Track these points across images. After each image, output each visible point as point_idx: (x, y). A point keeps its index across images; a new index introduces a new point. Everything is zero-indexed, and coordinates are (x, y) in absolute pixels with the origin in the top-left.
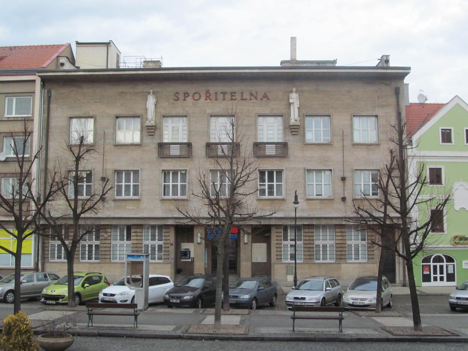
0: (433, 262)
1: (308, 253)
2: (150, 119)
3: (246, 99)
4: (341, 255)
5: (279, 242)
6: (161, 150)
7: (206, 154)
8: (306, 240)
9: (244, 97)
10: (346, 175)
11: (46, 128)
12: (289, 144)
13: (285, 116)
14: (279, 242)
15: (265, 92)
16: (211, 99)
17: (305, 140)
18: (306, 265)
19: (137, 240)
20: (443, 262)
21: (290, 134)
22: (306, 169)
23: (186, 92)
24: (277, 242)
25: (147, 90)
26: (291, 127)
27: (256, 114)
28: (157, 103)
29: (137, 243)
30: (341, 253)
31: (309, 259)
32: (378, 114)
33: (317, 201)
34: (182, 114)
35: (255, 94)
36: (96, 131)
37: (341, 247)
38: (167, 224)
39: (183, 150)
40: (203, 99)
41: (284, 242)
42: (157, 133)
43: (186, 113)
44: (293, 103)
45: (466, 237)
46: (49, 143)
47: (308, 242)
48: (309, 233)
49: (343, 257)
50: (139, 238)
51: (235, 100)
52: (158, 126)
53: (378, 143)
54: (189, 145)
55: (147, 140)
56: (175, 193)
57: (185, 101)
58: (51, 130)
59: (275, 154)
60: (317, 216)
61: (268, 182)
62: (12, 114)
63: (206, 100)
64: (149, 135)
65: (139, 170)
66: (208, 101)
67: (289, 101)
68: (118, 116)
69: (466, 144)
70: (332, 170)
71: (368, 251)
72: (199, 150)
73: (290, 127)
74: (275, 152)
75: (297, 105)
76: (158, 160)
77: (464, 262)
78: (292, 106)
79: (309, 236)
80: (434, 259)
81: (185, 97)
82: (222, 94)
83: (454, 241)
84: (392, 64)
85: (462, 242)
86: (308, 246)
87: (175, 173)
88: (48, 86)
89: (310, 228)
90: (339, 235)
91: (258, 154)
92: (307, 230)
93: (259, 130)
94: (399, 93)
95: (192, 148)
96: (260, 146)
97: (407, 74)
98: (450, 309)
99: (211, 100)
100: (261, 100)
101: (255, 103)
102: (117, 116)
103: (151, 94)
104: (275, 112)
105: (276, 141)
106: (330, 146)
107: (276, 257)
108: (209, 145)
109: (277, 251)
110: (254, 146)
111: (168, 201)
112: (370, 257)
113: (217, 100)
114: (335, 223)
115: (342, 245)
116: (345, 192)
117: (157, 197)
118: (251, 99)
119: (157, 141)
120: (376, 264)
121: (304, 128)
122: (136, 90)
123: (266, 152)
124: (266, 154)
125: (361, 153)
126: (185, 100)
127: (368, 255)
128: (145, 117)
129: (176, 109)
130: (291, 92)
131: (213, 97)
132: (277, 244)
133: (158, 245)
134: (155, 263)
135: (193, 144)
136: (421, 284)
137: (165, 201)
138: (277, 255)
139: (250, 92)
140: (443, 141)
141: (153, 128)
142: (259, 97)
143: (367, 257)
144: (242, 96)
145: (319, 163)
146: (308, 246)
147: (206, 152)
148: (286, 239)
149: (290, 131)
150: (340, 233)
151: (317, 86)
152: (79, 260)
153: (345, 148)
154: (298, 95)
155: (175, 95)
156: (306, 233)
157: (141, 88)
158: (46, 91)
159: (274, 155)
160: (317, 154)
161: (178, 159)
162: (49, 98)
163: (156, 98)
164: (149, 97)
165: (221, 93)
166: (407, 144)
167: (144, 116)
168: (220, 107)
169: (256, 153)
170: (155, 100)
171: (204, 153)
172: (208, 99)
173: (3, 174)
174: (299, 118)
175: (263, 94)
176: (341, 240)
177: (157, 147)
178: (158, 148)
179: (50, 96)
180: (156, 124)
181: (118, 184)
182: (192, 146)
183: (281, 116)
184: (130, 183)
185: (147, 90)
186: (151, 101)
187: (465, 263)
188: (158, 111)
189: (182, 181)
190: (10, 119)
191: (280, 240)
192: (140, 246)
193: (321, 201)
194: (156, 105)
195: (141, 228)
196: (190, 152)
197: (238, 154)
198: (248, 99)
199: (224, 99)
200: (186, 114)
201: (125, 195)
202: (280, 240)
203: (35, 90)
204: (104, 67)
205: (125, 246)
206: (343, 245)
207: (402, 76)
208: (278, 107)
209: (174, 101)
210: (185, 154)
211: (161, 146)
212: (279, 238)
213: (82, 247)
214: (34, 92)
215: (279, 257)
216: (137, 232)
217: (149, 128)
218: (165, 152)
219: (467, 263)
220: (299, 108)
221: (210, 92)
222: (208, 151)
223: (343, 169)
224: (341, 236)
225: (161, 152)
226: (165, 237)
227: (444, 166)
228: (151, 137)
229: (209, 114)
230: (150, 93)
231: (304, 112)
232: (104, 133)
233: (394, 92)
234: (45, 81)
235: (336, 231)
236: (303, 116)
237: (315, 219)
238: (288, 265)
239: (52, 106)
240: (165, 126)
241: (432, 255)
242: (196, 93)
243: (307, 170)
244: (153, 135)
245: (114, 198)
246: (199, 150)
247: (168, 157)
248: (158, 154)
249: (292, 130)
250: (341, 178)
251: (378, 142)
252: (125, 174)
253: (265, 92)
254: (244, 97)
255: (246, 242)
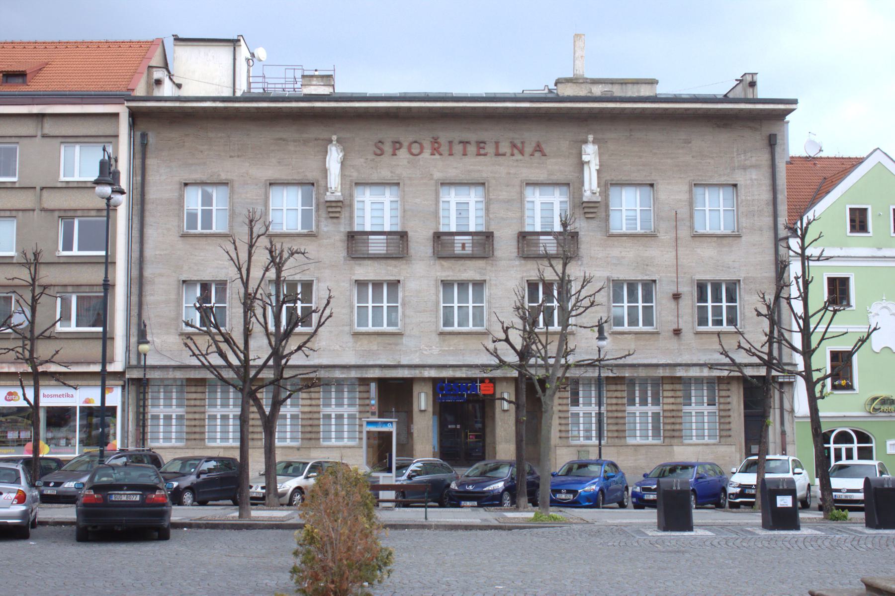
0: (835, 443)
1: (615, 428)
2: (333, 189)
3: (504, 155)
4: (674, 430)
5: (564, 408)
6: (354, 245)
7: (434, 252)
8: (611, 404)
9: (501, 151)
10: (681, 290)
11: (139, 202)
12: (581, 234)
13: (573, 185)
14: (564, 408)
15: (538, 142)
16: (442, 153)
17: (609, 228)
18: (612, 448)
19: (310, 405)
20: (852, 442)
21: (582, 216)
22: (611, 279)
23: (396, 140)
24: (560, 408)
25: (581, 137)
26: (584, 205)
27: (522, 182)
28: (344, 159)
29: (310, 412)
30: (673, 427)
31: (617, 437)
32: (653, 180)
33: (631, 335)
34: (390, 180)
35: (519, 145)
36: (233, 210)
37: (673, 417)
38: (366, 376)
39: (392, 245)
40: (426, 154)
41: (325, 408)
42: (345, 214)
43: (396, 178)
44: (589, 162)
45: (893, 398)
46: (145, 230)
47: (614, 408)
48: (616, 393)
49: (676, 434)
50: (314, 402)
51: (485, 155)
52: (347, 202)
53: (737, 233)
54: (403, 235)
55: (327, 227)
56: (377, 322)
57: (395, 157)
58: (149, 207)
59: (384, 252)
60: (451, 363)
61: (712, 302)
62: (73, 176)
63: (432, 154)
64: (332, 218)
65: (313, 280)
66: (437, 156)
67: (581, 158)
68: (273, 182)
69: (893, 234)
70: (657, 282)
71: (720, 423)
72: (505, 245)
73: (582, 204)
74: (385, 248)
75: (596, 165)
76: (348, 262)
77: (889, 443)
78: (586, 168)
79: (616, 397)
80: (836, 437)
81: (395, 149)
82: (461, 144)
83: (871, 405)
84: (762, 92)
85: (885, 407)
86: (615, 414)
87: (377, 285)
88: (142, 126)
89: (619, 383)
90: (670, 395)
91: (525, 252)
92: (613, 387)
93: (482, 209)
94: (775, 144)
95: (407, 240)
96: (529, 237)
97: (790, 111)
98: (761, 524)
99: (441, 154)
100: (531, 155)
101: (521, 160)
102: (271, 182)
103: (334, 143)
104: (556, 178)
105: (387, 229)
106: (653, 238)
107: (558, 435)
108: (438, 236)
109: (560, 424)
110: (518, 238)
111: (367, 336)
112: (724, 433)
113: (452, 155)
114: (662, 375)
115: (674, 414)
116: (680, 320)
117: (347, 329)
118: (513, 155)
119: (344, 228)
120: (734, 447)
121: (607, 206)
122: (305, 136)
123: (455, 249)
124: (370, 252)
125: (707, 251)
126: (394, 154)
127: (721, 430)
128: (323, 185)
129: (379, 171)
130: (586, 142)
131: (444, 149)
132: (560, 411)
133: (652, 413)
134: (344, 447)
135: (410, 234)
136: (814, 480)
137: (361, 337)
138: (560, 431)
139: (511, 142)
140: (853, 229)
141: (340, 204)
142: (528, 149)
143: (718, 434)
144: (497, 148)
145: (634, 269)
146: (615, 414)
147: (434, 248)
148: (632, 402)
149: (582, 212)
150: (670, 392)
151: (631, 130)
152: (205, 443)
153: (679, 242)
154: (597, 147)
155: (376, 145)
156: (611, 393)
157: (316, 131)
158: (138, 134)
159: (555, 254)
160: (629, 252)
161: (383, 262)
162: (144, 146)
163: (344, 150)
164: (330, 149)
165: (461, 142)
166: (789, 235)
167: (322, 183)
168: (455, 167)
169: (523, 251)
170: (341, 155)
171: (430, 251)
172: (437, 154)
173: (59, 287)
174: (599, 190)
175: (534, 145)
176: (673, 404)
177: (346, 238)
178: (348, 240)
179: (147, 144)
180: (344, 198)
181: (530, 305)
182: (407, 236)
183: (568, 184)
184: (368, 303)
185: (325, 135)
186: (334, 157)
187: (891, 445)
188: (346, 173)
189: (645, 300)
190: (71, 185)
191: (565, 405)
192: (316, 416)
193: (638, 335)
194: (342, 163)
195: (623, 383)
196: (405, 248)
197: (491, 252)
198: (508, 154)
199: (465, 154)
200: (398, 180)
201: (643, 325)
202: (565, 405)
203: (118, 132)
204: (227, 93)
205: (694, 414)
206: (677, 413)
207: (779, 116)
208: (558, 167)
209: (374, 157)
210: (396, 252)
211: (353, 237)
212: (565, 401)
213: (209, 419)
214: (117, 136)
215: (563, 435)
216: (676, 390)
217: (330, 204)
218: (359, 248)
219: (894, 444)
220: (598, 171)
221: (439, 140)
222: (438, 247)
223: (676, 280)
224: (672, 397)
225: (352, 247)
226: (623, 402)
227: (853, 274)
228: (335, 221)
229: (438, 180)
230: (331, 141)
231: (607, 177)
232: (676, 214)
233: (766, 142)
234: (135, 116)
235: (664, 389)
236: (607, 184)
237: (627, 368)
238: (580, 449)
239: (151, 162)
240: (528, 202)
241: (833, 431)
242: (415, 142)
243: (613, 280)
244: (337, 218)
245: (182, 330)
246: (505, 245)
247: (365, 258)
248: (348, 251)
249: (586, 210)
250: (671, 294)
251: (738, 232)
252: (628, 288)
253: (538, 142)
254: (501, 151)
255: (423, 408)
